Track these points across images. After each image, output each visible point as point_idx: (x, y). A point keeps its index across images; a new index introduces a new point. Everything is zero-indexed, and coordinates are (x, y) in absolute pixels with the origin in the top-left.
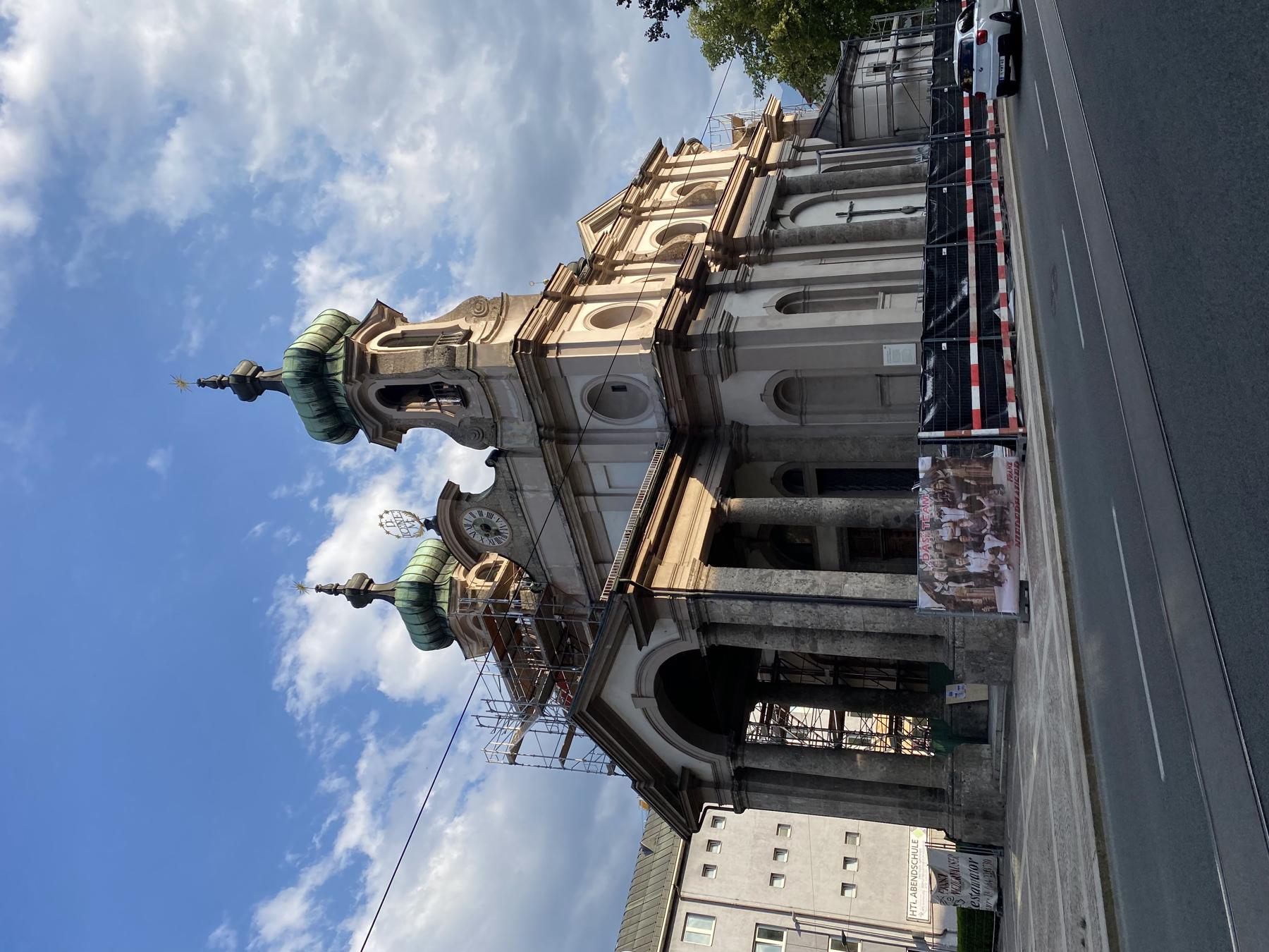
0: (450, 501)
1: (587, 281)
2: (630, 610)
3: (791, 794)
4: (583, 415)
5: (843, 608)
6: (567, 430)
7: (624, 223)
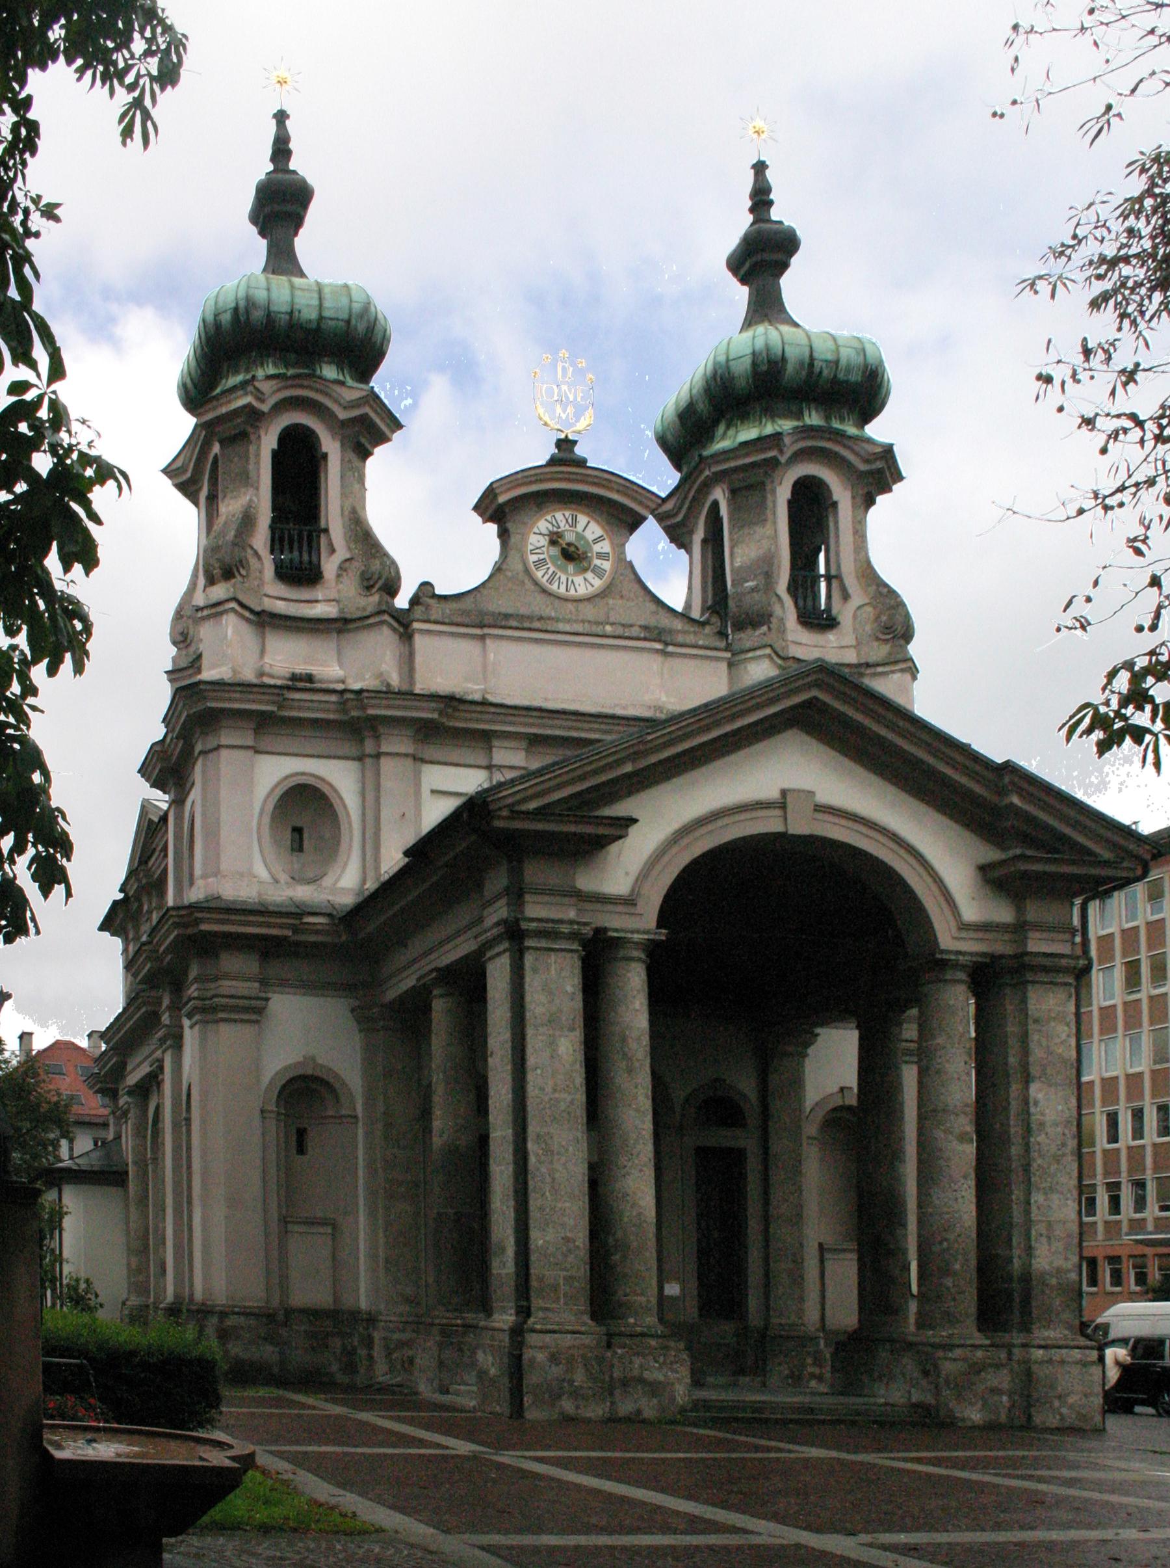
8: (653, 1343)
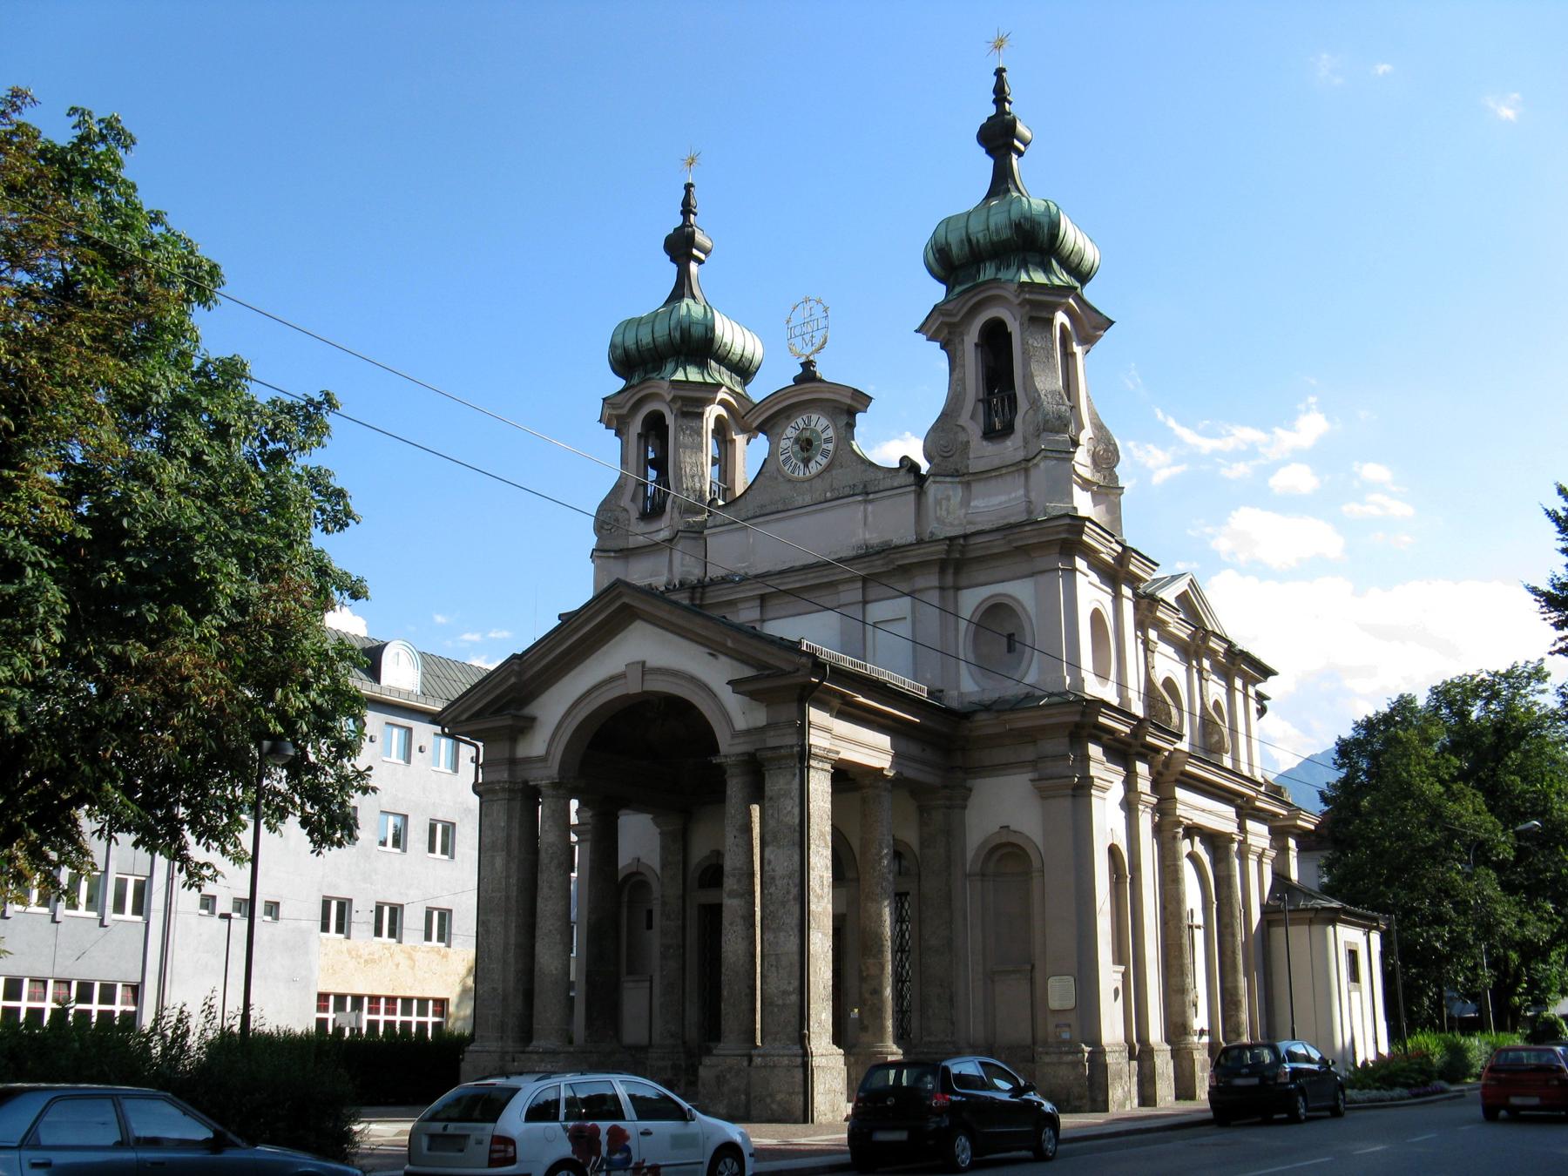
0: (849, 401)
1: (1138, 598)
2: (782, 673)
3: (509, 854)
4: (971, 600)
5: (796, 931)
6: (957, 572)
7: (1183, 632)
8: (535, 1057)
